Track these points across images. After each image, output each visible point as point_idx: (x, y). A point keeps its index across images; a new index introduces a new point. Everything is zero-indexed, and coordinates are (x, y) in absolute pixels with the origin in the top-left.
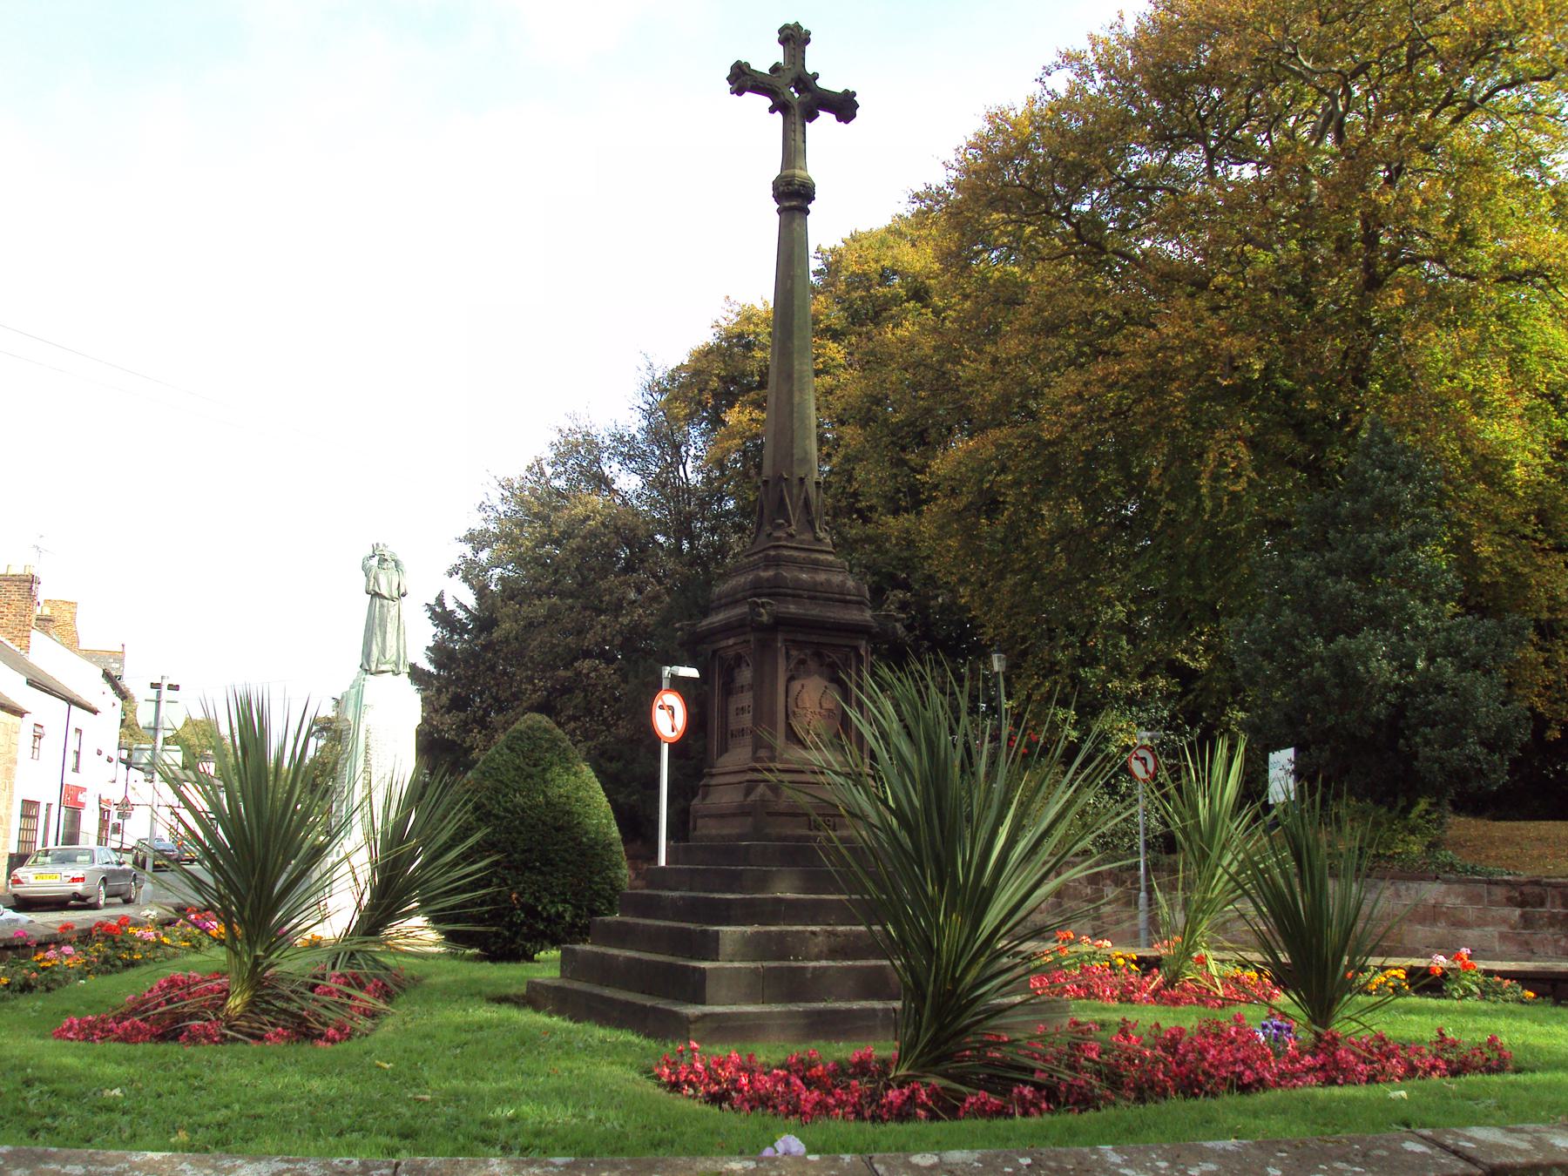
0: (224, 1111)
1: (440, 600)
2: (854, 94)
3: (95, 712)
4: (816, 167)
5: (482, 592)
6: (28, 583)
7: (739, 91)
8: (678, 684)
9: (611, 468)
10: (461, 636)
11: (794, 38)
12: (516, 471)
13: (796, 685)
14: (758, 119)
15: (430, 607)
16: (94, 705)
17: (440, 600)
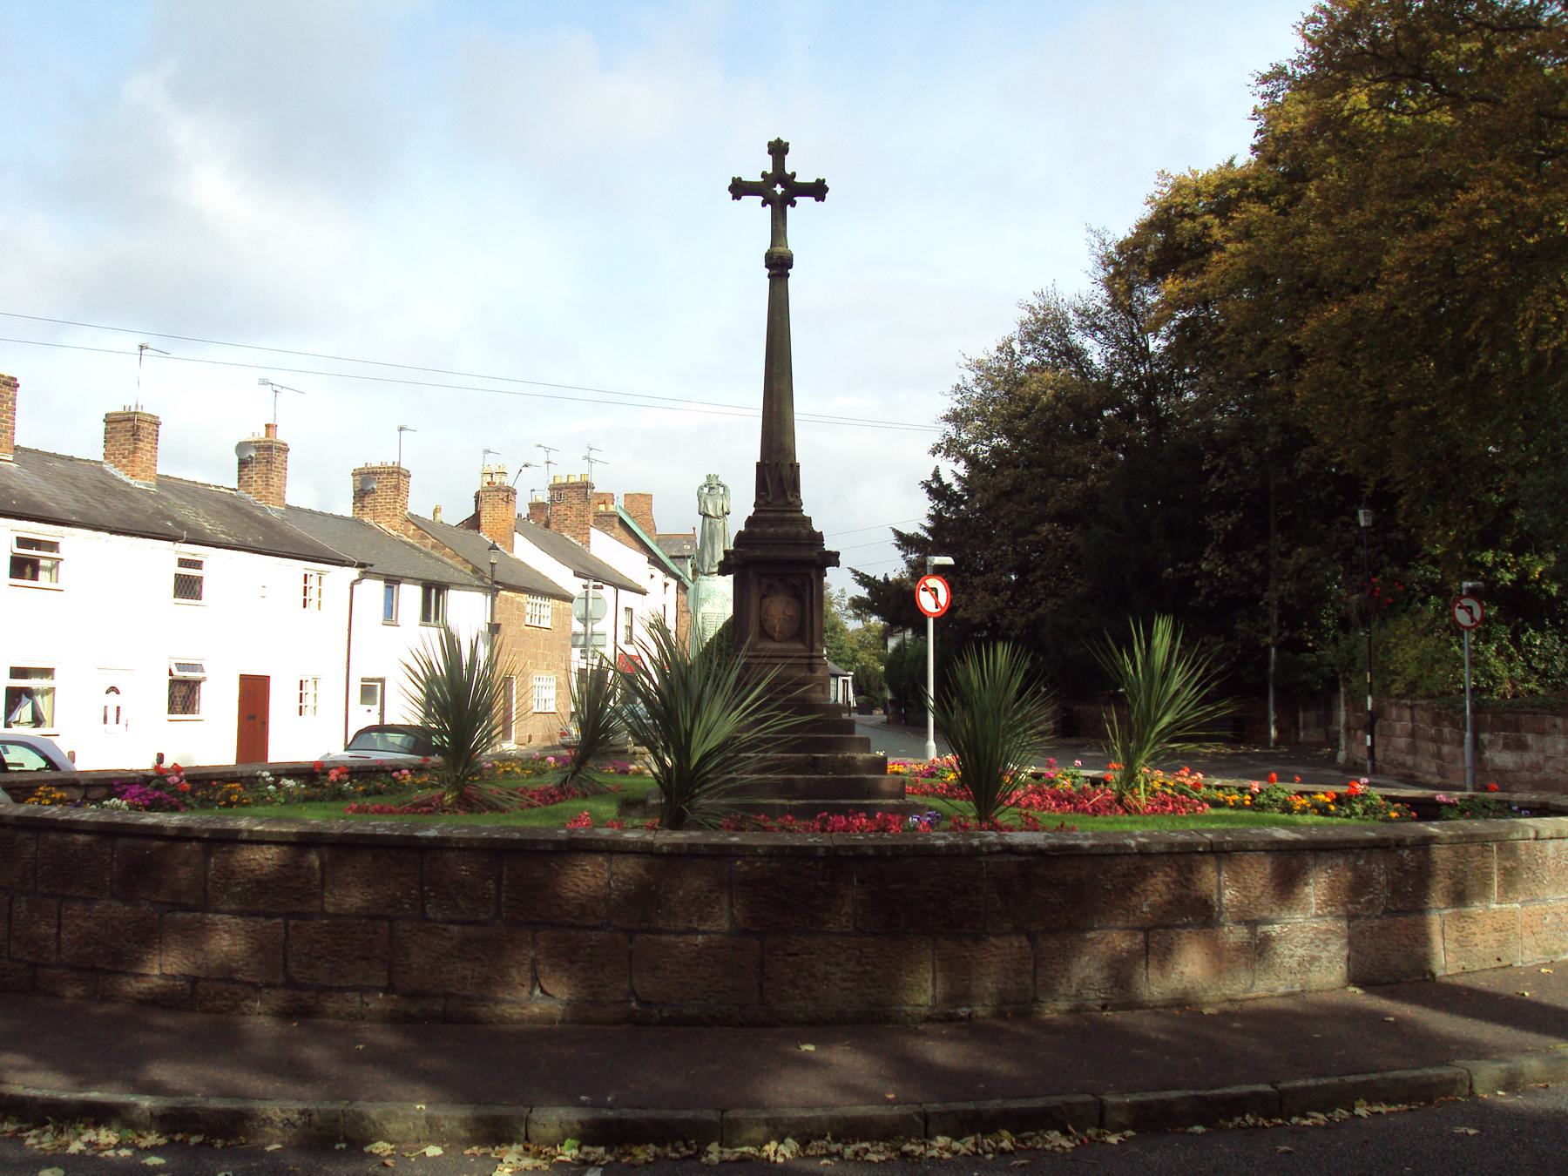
1: (936, 476)
3: (644, 593)
4: (795, 241)
5: (972, 462)
6: (584, 487)
7: (737, 196)
8: (940, 571)
9: (1079, 339)
10: (957, 506)
12: (985, 347)
13: (767, 601)
14: (755, 211)
15: (927, 485)
17: (936, 476)
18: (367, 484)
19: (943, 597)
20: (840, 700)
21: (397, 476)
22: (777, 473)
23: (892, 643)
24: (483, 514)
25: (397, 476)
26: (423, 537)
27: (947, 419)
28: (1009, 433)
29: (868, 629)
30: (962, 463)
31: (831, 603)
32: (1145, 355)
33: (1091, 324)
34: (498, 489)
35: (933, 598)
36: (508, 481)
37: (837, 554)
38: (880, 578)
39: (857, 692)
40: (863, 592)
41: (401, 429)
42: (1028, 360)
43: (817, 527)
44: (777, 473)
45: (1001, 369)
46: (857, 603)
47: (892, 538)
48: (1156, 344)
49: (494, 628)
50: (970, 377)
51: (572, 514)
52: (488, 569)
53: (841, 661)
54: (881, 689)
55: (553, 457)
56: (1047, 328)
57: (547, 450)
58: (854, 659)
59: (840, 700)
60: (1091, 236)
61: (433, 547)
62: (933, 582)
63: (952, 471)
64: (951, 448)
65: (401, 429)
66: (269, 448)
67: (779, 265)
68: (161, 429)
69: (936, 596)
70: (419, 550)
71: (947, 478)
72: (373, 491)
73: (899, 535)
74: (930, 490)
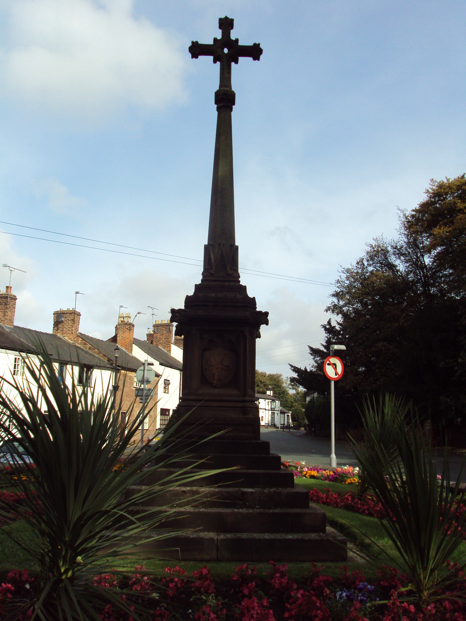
0: (137, 544)
1: (329, 323)
2: (259, 44)
4: (236, 85)
5: (345, 316)
8: (337, 354)
9: (393, 259)
10: (338, 336)
11: (226, 24)
12: (351, 263)
14: (209, 67)
15: (324, 327)
16: (133, 367)
17: (329, 323)
18: (60, 318)
19: (340, 369)
20: (286, 423)
21: (74, 315)
22: (221, 254)
23: (308, 399)
24: (118, 335)
25: (74, 315)
26: (85, 344)
27: (333, 295)
28: (361, 302)
29: (298, 393)
30: (340, 316)
31: (283, 382)
32: (423, 267)
33: (399, 253)
34: (126, 324)
35: (334, 370)
36: (131, 321)
37: (266, 314)
38: (303, 368)
39: (293, 420)
40: (295, 375)
41: (77, 293)
42: (370, 269)
43: (250, 294)
44: (221, 254)
45: (357, 272)
46: (292, 380)
47: (308, 350)
48: (427, 260)
49: (116, 388)
50: (344, 276)
51: (163, 337)
52: (114, 359)
53: (286, 407)
54: (303, 419)
55: (155, 312)
56: (378, 254)
57: (153, 309)
58: (292, 406)
59: (286, 423)
60: (399, 212)
61: (90, 349)
62: (333, 360)
63: (337, 320)
64: (335, 309)
65: (77, 293)
66: (7, 297)
67: (225, 100)
68: (16, 309)
69: (335, 369)
70: (82, 350)
71: (334, 324)
72: (62, 322)
73: (311, 349)
74: (326, 329)
